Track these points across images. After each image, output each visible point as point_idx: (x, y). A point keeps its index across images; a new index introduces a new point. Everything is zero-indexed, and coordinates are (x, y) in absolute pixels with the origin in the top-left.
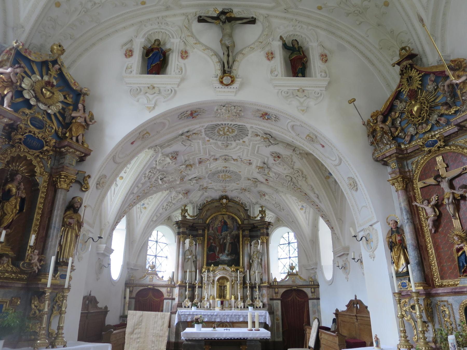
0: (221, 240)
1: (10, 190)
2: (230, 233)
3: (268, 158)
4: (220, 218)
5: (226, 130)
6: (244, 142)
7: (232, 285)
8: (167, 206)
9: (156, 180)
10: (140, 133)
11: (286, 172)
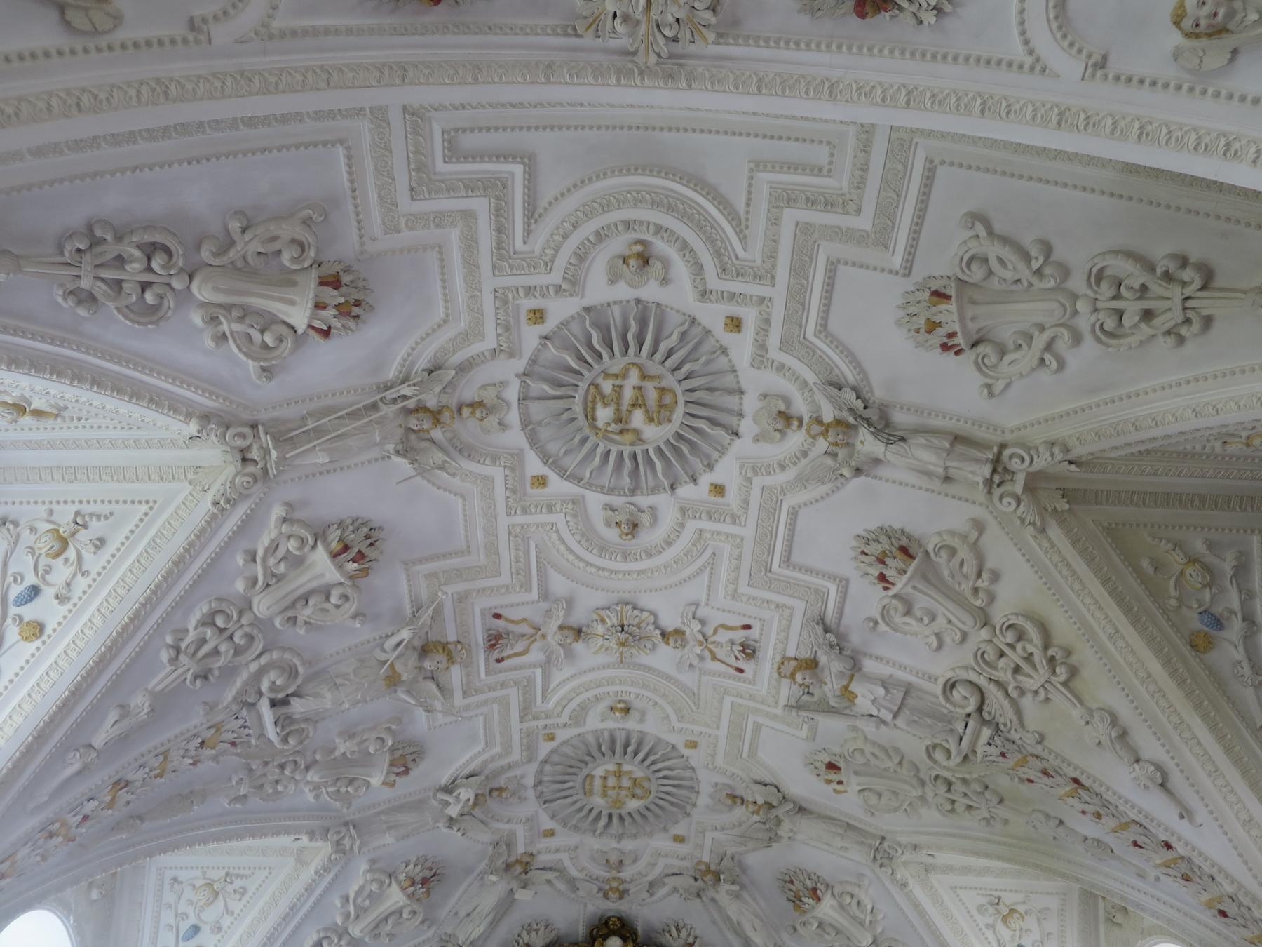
3: (844, 584)
5: (628, 394)
6: (719, 490)
11: (944, 666)
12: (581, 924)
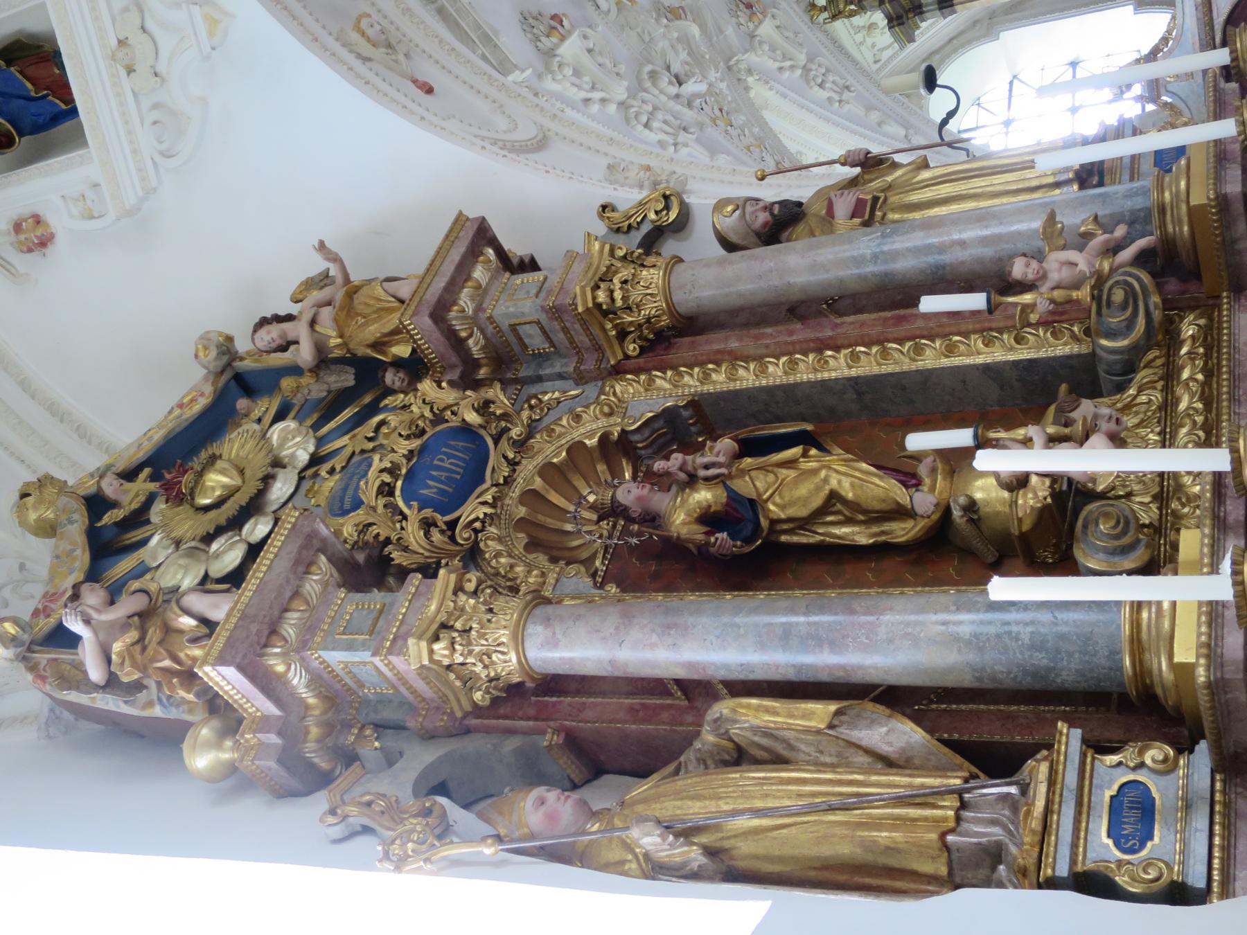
1: (709, 519)
8: (828, 85)
9: (690, 105)
10: (366, 60)
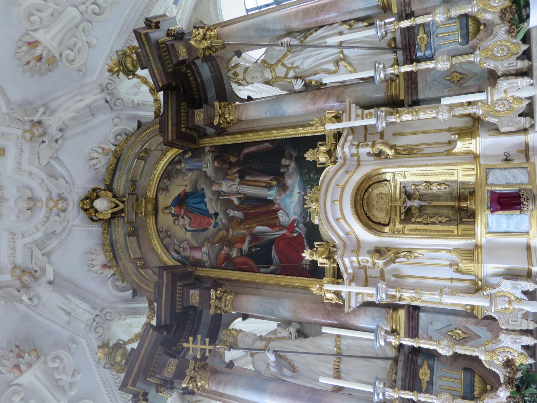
0: (233, 218)
2: (211, 183)
4: (165, 219)
7: (398, 153)
12: (91, 228)
